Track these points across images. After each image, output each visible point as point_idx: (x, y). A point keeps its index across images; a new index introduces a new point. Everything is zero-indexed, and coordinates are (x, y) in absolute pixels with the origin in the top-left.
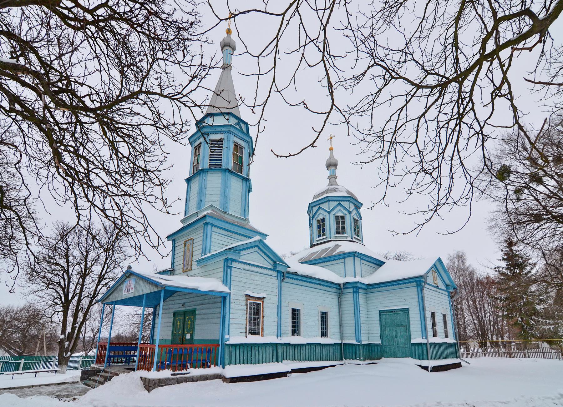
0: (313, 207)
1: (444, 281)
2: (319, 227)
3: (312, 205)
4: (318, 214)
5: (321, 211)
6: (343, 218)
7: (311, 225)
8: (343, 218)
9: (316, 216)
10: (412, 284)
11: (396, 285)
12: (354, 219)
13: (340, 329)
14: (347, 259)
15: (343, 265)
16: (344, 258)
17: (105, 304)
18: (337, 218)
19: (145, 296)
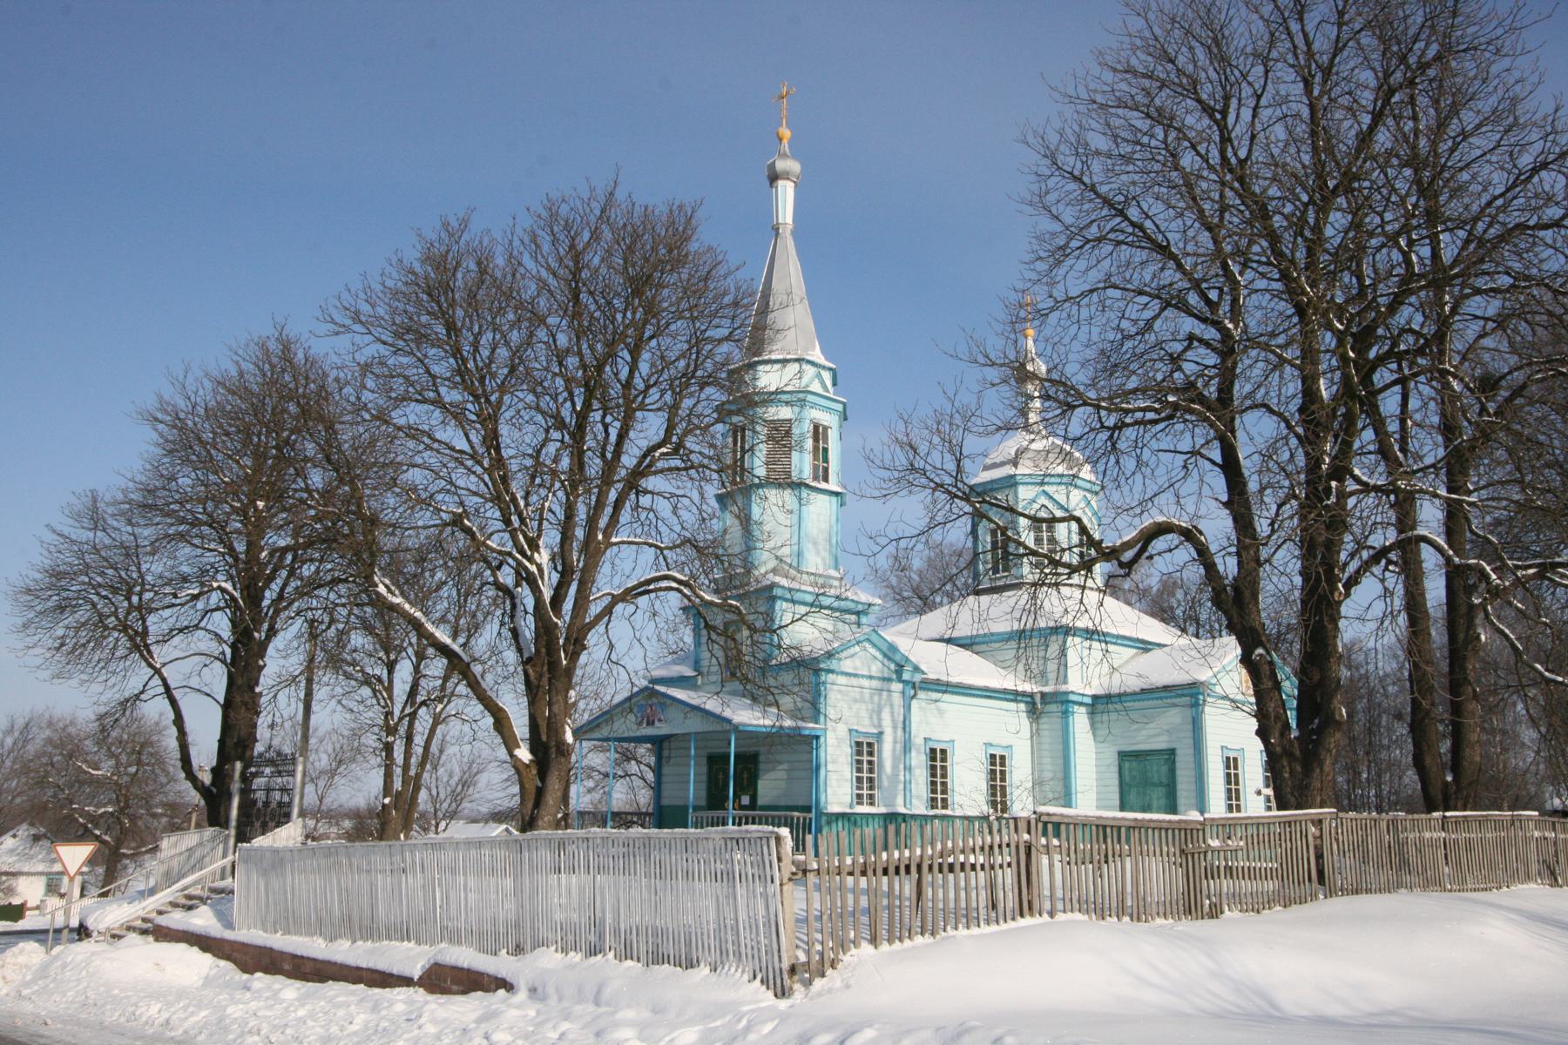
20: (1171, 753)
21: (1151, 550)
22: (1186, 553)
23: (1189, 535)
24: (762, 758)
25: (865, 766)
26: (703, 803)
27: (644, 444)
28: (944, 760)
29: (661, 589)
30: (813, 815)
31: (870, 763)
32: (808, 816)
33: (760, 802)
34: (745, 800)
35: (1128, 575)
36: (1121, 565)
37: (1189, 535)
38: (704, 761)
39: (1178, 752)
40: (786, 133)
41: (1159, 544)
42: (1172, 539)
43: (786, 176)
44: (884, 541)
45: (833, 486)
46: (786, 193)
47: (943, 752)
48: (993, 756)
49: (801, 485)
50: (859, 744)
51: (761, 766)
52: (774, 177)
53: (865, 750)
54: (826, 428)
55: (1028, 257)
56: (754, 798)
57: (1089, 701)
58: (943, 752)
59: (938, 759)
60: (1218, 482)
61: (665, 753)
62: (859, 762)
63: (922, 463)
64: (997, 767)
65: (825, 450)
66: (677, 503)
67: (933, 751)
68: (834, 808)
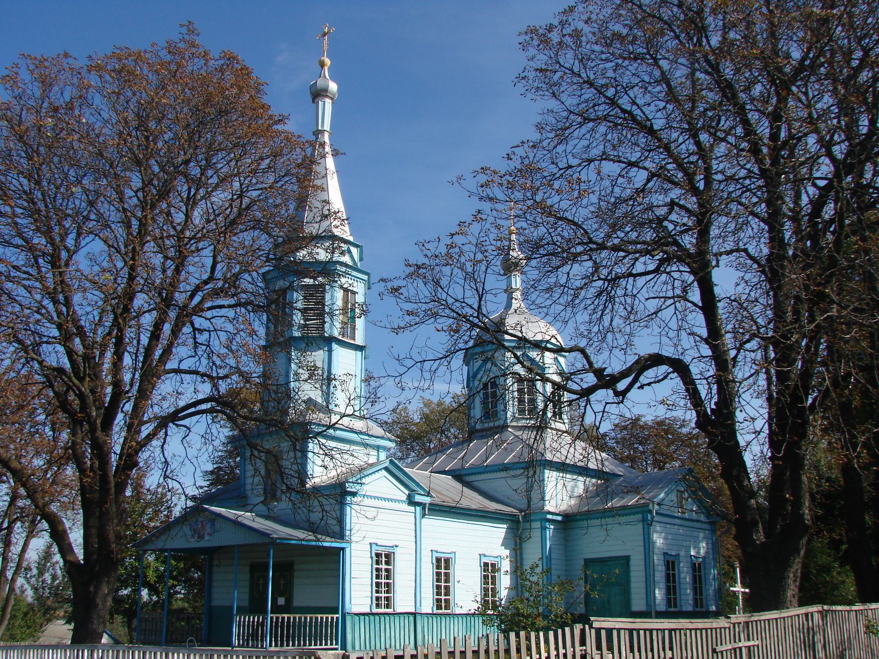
20: (627, 559)
21: (643, 379)
22: (675, 382)
23: (680, 368)
24: (296, 567)
25: (384, 573)
26: (246, 603)
27: (194, 281)
30: (339, 616)
31: (387, 570)
32: (335, 616)
33: (297, 603)
34: (281, 601)
36: (617, 394)
37: (680, 368)
38: (247, 569)
39: (632, 558)
40: (328, 61)
41: (650, 374)
42: (663, 369)
44: (409, 363)
45: (359, 340)
46: (327, 107)
47: (447, 561)
48: (486, 564)
50: (378, 555)
51: (296, 574)
52: (318, 94)
53: (383, 560)
56: (289, 600)
59: (443, 566)
60: (698, 320)
62: (378, 570)
63: (444, 296)
64: (489, 571)
66: (228, 335)
67: (438, 560)
68: (356, 609)
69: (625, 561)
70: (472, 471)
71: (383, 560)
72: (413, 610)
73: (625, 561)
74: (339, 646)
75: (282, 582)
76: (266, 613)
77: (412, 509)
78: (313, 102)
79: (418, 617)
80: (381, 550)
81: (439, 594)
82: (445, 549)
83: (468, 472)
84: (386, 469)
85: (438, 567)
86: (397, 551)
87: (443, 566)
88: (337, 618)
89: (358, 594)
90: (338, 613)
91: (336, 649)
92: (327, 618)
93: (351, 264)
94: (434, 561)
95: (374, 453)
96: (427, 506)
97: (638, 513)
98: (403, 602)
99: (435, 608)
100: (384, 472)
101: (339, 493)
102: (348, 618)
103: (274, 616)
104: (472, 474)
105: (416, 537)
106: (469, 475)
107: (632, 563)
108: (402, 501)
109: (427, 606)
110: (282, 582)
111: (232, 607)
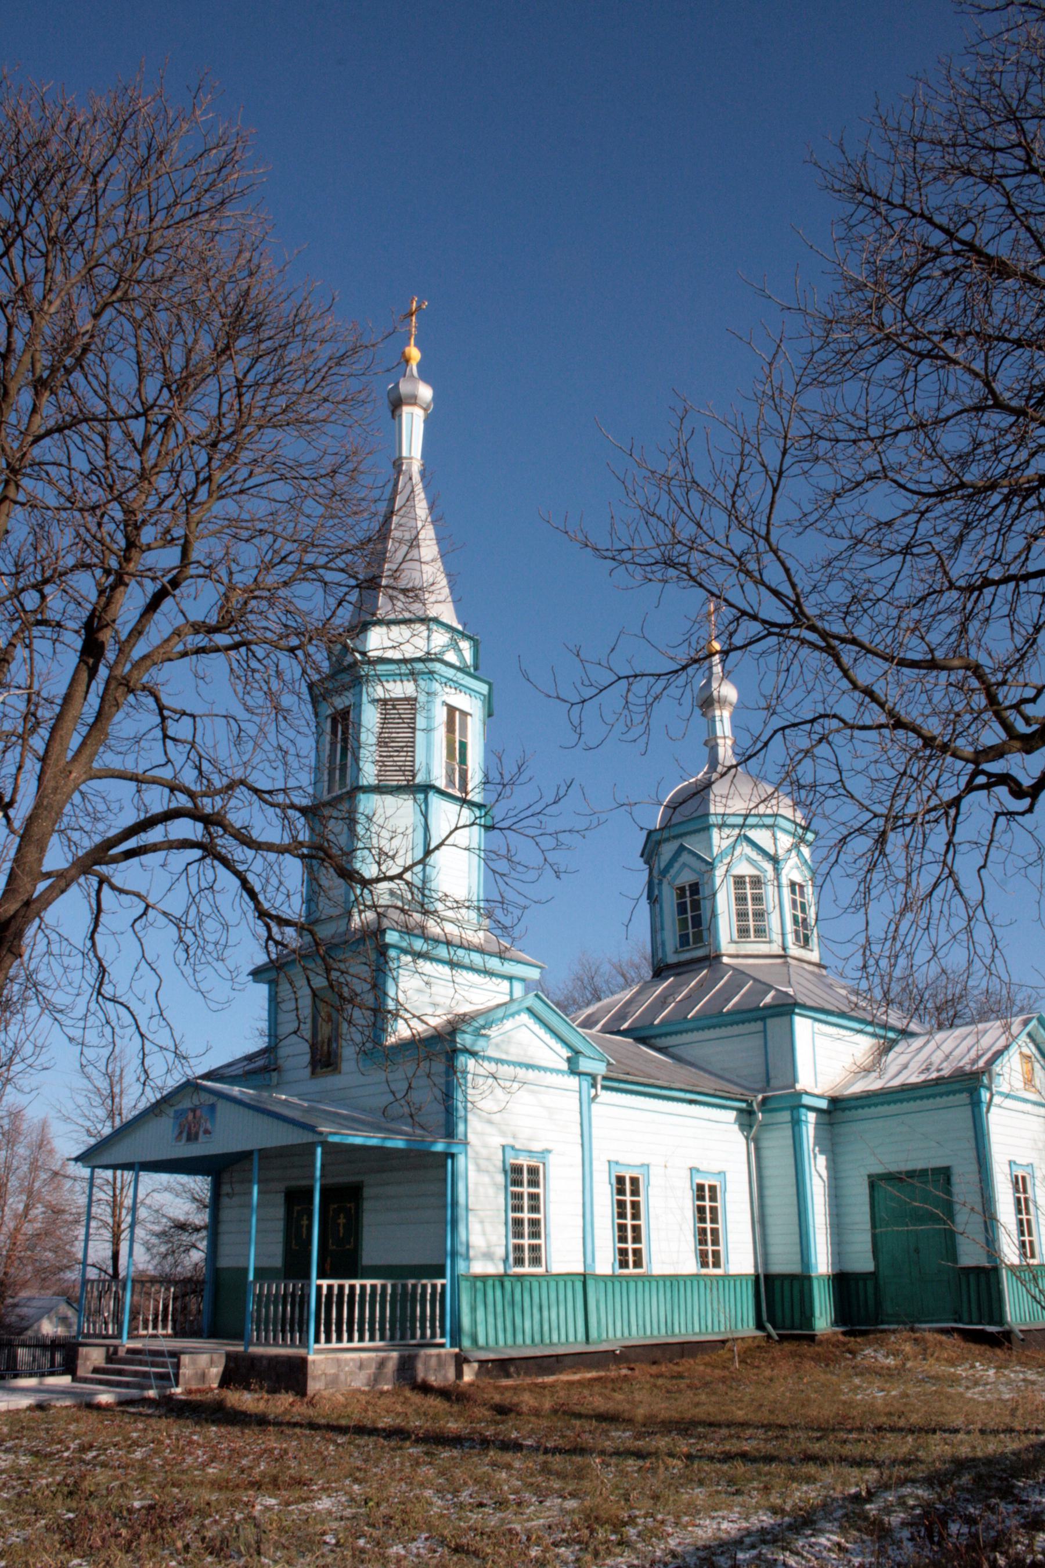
0: (659, 843)
1: (762, 1206)
2: (682, 908)
3: (656, 837)
4: (677, 866)
5: (685, 857)
6: (743, 932)
7: (653, 899)
8: (757, 882)
9: (673, 871)
10: (958, 1096)
11: (915, 1099)
12: (793, 884)
13: (980, 1172)
14: (769, 1021)
15: (757, 1041)
16: (763, 1019)
17: (93, 1168)
18: (739, 881)
19: (256, 1157)
24: (367, 1192)
26: (278, 1262)
28: (635, 1192)
29: (154, 848)
30: (447, 1281)
32: (439, 1282)
35: (1030, 810)
38: (280, 1199)
40: (414, 353)
43: (413, 400)
48: (701, 1188)
49: (427, 788)
51: (367, 1205)
54: (464, 714)
55: (840, 231)
57: (823, 1104)
58: (635, 1181)
59: (628, 1191)
61: (226, 1189)
64: (706, 1201)
65: (463, 746)
69: (944, 1175)
70: (664, 1030)
71: (523, 1179)
72: (581, 1270)
73: (944, 1175)
74: (446, 1340)
75: (342, 1220)
76: (308, 1276)
77: (573, 1081)
78: (393, 417)
79: (590, 1283)
80: (524, 1161)
81: (623, 1239)
82: (630, 1158)
83: (658, 1031)
84: (530, 1010)
85: (621, 1191)
86: (552, 1160)
87: (628, 1191)
88: (443, 1286)
89: (483, 1236)
90: (443, 1276)
91: (442, 1345)
92: (352, 1288)
93: (458, 664)
94: (614, 1181)
95: (505, 984)
96: (599, 1078)
97: (961, 1091)
98: (563, 1254)
99: (617, 1265)
100: (525, 1018)
101: (443, 1050)
102: (464, 1285)
103: (325, 1283)
104: (670, 1034)
105: (582, 1136)
106: (660, 1036)
107: (955, 1179)
108: (558, 1071)
109: (605, 1263)
110: (342, 1220)
111: (246, 1270)
